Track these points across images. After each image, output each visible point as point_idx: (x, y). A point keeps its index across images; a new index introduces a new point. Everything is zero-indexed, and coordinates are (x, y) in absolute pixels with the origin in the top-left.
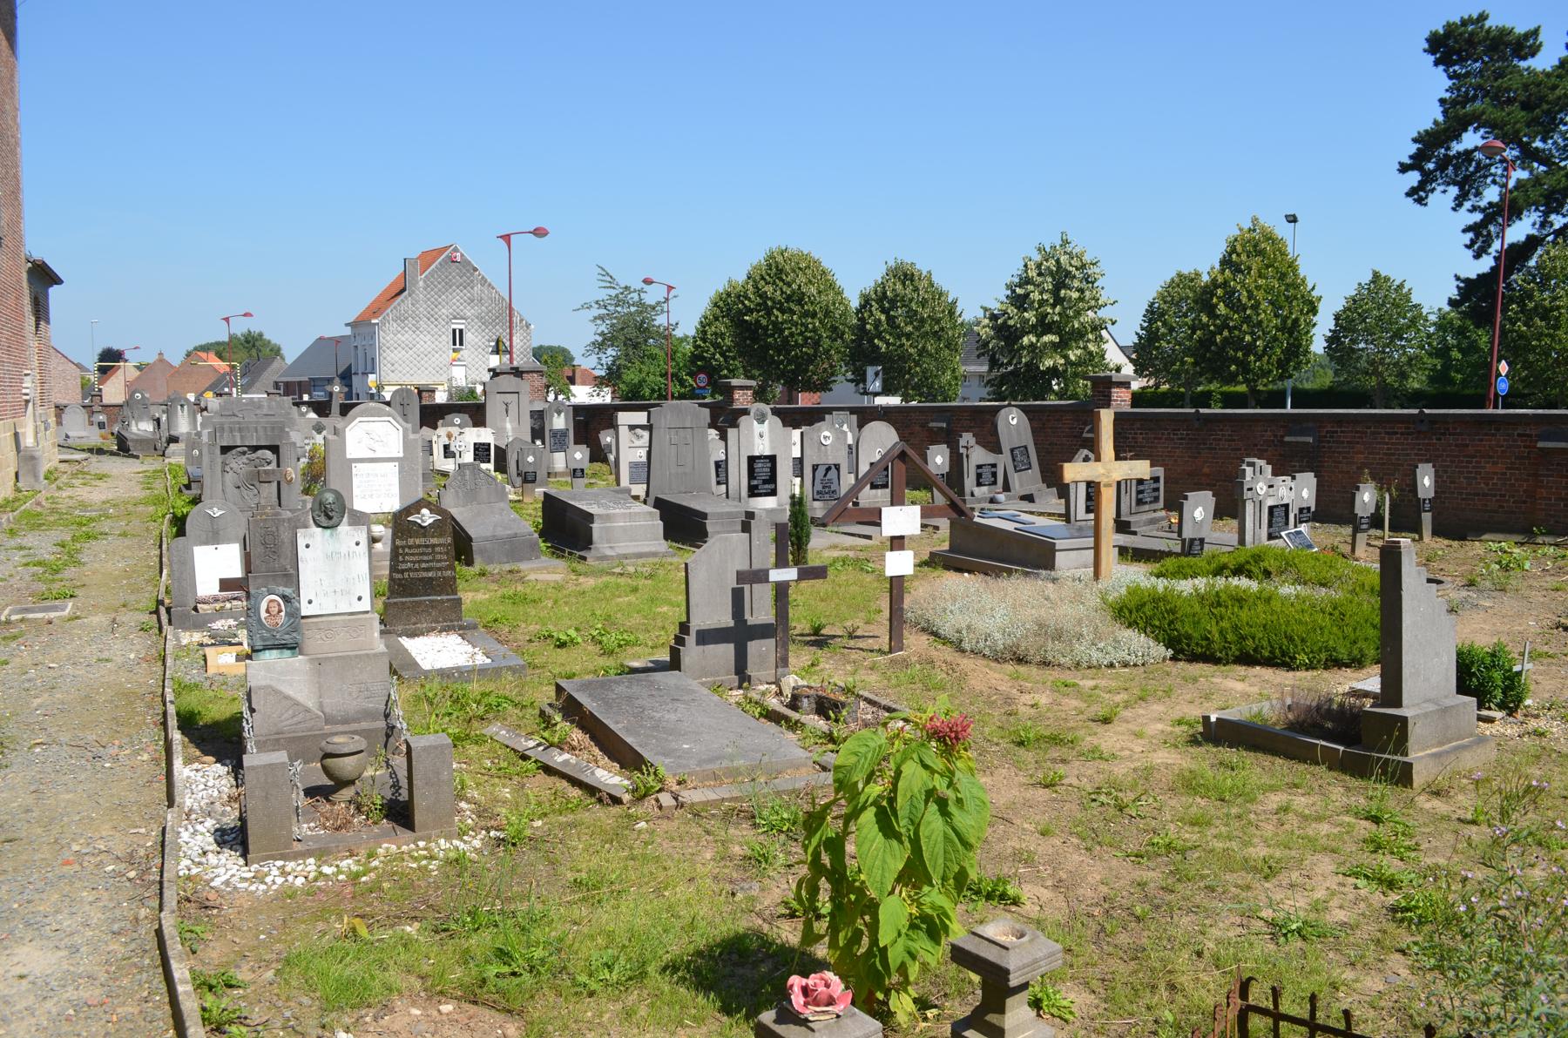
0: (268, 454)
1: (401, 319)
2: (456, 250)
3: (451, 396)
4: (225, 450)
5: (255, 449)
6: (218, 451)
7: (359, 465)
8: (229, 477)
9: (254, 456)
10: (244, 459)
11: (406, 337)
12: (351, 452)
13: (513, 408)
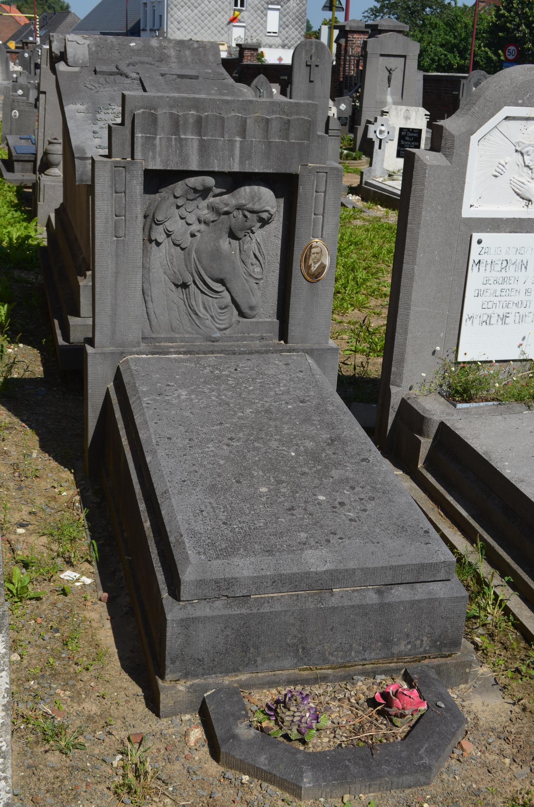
0: (266, 198)
3: (230, 53)
4: (157, 181)
5: (233, 181)
6: (137, 184)
7: (488, 238)
8: (162, 255)
9: (229, 200)
10: (202, 208)
12: (477, 202)
13: (397, 76)
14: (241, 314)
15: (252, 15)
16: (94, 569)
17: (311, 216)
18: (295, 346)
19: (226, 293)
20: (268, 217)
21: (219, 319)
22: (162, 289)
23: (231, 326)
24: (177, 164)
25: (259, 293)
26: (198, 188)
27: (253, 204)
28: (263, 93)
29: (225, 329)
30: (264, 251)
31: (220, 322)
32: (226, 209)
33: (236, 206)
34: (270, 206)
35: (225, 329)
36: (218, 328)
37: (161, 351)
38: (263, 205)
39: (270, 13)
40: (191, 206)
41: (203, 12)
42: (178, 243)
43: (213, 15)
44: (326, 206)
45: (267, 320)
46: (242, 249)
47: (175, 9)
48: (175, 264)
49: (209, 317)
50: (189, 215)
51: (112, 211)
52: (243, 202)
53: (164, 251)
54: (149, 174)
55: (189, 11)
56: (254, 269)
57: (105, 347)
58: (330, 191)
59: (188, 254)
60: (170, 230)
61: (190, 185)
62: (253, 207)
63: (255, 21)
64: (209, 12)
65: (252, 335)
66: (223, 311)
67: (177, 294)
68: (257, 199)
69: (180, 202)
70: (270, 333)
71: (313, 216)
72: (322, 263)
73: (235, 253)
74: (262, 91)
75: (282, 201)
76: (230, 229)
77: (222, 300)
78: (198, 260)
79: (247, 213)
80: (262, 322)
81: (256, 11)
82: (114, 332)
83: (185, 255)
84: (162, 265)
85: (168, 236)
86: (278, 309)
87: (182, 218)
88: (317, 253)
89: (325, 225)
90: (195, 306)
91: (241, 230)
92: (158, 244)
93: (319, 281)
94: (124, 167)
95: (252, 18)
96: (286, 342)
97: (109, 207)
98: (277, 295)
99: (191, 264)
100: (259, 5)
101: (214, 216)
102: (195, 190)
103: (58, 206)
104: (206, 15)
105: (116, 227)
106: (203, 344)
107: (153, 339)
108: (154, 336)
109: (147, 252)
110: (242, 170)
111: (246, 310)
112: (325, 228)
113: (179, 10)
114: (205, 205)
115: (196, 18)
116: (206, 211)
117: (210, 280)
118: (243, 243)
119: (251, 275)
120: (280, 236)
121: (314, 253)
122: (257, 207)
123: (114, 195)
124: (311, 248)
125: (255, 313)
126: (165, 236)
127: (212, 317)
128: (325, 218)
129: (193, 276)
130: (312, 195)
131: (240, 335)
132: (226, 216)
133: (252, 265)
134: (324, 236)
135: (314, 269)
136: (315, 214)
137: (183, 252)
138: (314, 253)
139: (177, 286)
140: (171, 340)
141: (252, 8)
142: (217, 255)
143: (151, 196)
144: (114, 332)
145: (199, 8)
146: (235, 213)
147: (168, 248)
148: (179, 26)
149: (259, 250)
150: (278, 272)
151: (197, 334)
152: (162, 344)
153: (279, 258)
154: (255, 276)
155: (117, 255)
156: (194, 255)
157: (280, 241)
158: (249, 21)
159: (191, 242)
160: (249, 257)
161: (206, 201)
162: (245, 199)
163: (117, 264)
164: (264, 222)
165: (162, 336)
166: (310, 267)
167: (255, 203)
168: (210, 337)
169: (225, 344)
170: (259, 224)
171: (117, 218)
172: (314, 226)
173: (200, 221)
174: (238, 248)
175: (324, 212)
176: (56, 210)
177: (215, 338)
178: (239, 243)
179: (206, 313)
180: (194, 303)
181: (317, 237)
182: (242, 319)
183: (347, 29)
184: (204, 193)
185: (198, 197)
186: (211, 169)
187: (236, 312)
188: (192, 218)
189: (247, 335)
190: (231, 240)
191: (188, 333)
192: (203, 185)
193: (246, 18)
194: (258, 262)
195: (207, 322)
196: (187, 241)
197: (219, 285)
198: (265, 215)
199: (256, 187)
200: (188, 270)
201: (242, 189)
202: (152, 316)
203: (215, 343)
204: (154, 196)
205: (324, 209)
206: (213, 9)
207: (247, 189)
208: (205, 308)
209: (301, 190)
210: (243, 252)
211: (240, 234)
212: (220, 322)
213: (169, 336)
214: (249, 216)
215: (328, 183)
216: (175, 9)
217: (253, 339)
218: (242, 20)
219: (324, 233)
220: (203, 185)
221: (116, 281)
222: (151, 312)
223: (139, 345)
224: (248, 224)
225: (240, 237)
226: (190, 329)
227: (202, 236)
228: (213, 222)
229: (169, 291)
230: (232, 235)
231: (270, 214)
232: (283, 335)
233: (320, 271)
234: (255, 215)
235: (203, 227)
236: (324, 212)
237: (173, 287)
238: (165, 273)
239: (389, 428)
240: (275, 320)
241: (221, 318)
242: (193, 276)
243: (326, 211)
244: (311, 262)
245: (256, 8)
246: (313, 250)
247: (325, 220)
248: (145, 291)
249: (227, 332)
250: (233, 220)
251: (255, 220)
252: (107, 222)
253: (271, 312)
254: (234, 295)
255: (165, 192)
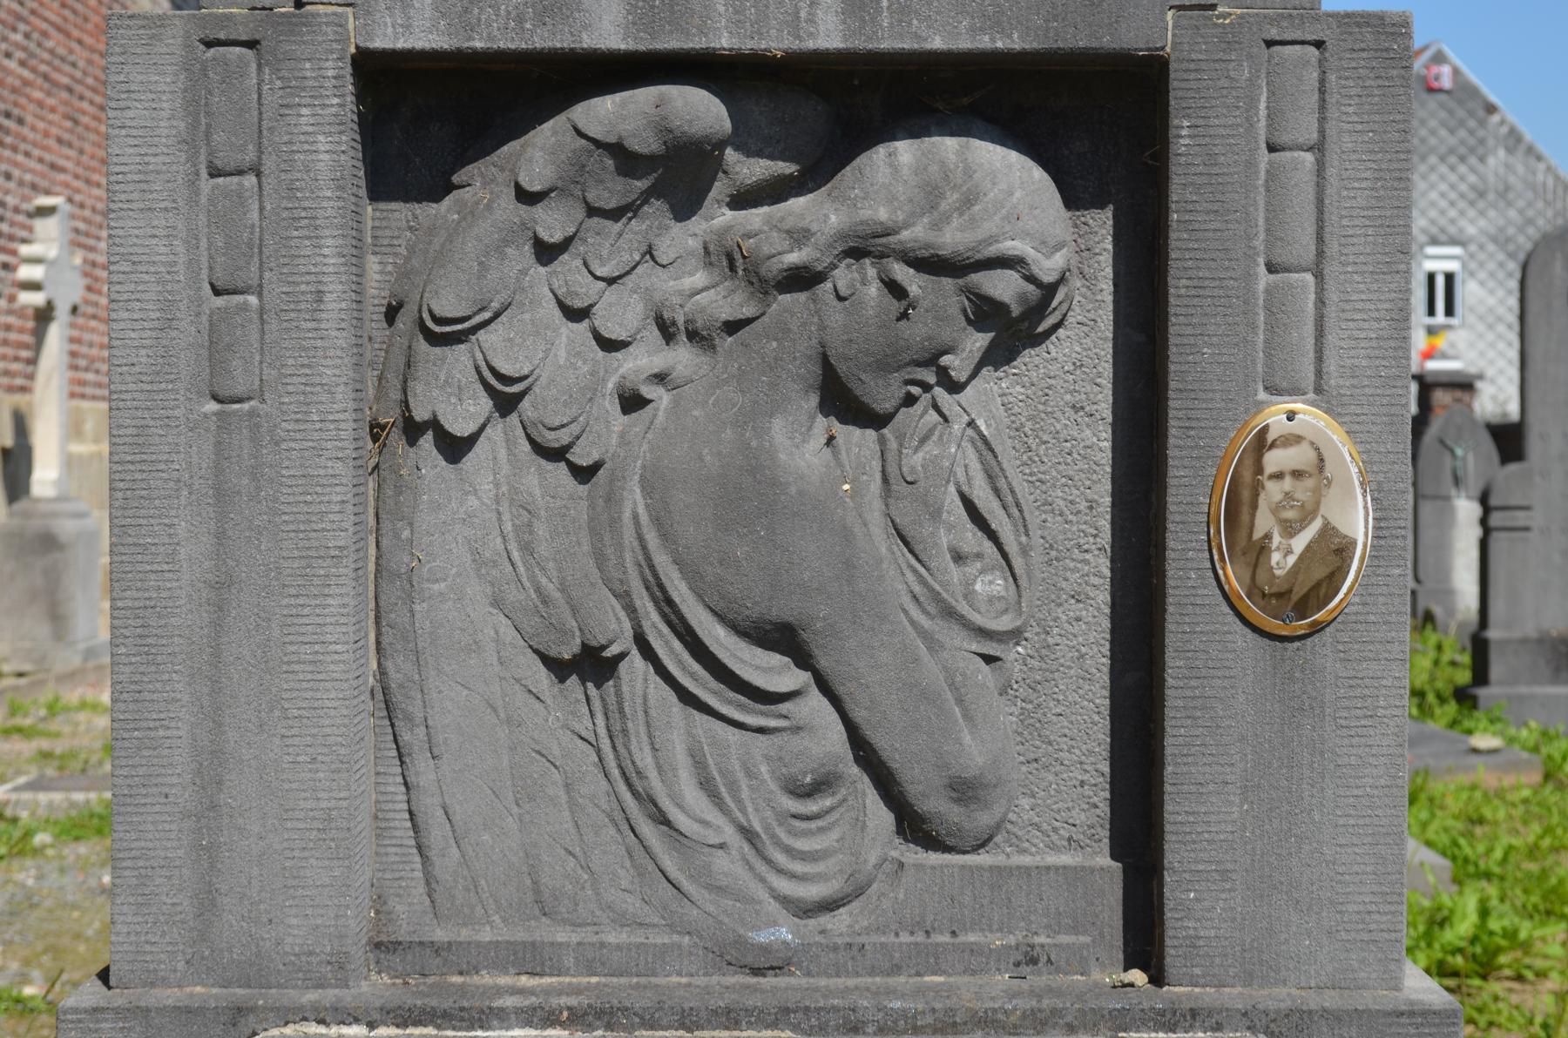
0: (1002, 195)
6: (322, 135)
8: (478, 506)
10: (679, 258)
14: (914, 827)
15: (1481, 336)
17: (1250, 277)
18: (1206, 995)
19: (816, 702)
20: (1022, 298)
21: (788, 851)
22: (482, 682)
23: (859, 892)
24: (520, 20)
25: (1006, 716)
26: (635, 145)
27: (936, 226)
28: (1464, 459)
29: (829, 906)
30: (1022, 489)
31: (798, 867)
32: (793, 258)
33: (842, 236)
34: (1026, 234)
35: (829, 906)
36: (785, 901)
37: (447, 1004)
38: (988, 227)
40: (611, 246)
42: (553, 439)
44: (1332, 218)
45: (1052, 859)
46: (892, 470)
48: (543, 550)
49: (730, 834)
50: (611, 294)
51: (192, 264)
52: (883, 214)
53: (486, 486)
54: (385, 81)
56: (969, 584)
57: (165, 983)
58: (1343, 142)
59: (608, 499)
60: (506, 368)
61: (594, 131)
62: (931, 237)
63: (1491, 354)
65: (972, 938)
66: (812, 807)
67: (564, 710)
68: (952, 198)
69: (552, 222)
70: (1075, 929)
71: (1263, 279)
72: (1328, 531)
73: (855, 493)
74: (1459, 452)
75: (1101, 222)
76: (825, 361)
77: (796, 742)
78: (657, 521)
79: (902, 273)
80: (1026, 871)
81: (1490, 327)
82: (207, 903)
83: (592, 506)
84: (479, 561)
85: (506, 404)
86: (1114, 803)
87: (575, 314)
88: (1297, 474)
89: (1330, 323)
90: (652, 774)
91: (885, 366)
92: (455, 448)
93: (1317, 629)
94: (251, 44)
95: (1481, 345)
96: (1157, 979)
97: (180, 249)
98: (1104, 723)
99: (620, 547)
101: (739, 297)
102: (624, 158)
105: (217, 348)
106: (701, 981)
107: (437, 949)
108: (440, 935)
109: (399, 491)
110: (860, 44)
111: (934, 804)
112: (1331, 339)
114: (692, 243)
116: (699, 278)
117: (721, 631)
118: (901, 438)
119: (950, 613)
120: (1105, 409)
121: (1278, 476)
122: (953, 239)
123: (206, 185)
124: (1261, 443)
125: (984, 819)
126: (486, 404)
127: (748, 834)
128: (1330, 285)
129: (631, 610)
130: (1251, 164)
131: (905, 938)
132: (802, 297)
133: (959, 558)
134: (1333, 382)
135: (1284, 558)
136: (1271, 268)
137: (583, 490)
138: (1278, 476)
139: (559, 668)
140: (532, 959)
141: (1481, 318)
142: (751, 493)
143: (417, 208)
144: (207, 903)
146: (844, 276)
147: (506, 469)
149: (991, 477)
150: (1103, 597)
151: (672, 927)
152: (486, 979)
153: (1105, 524)
154: (978, 619)
155: (222, 495)
156: (634, 499)
157: (1107, 434)
159: (622, 435)
160: (936, 514)
161: (697, 224)
162: (891, 199)
163: (220, 535)
164: (1013, 331)
165: (486, 935)
166: (1262, 549)
167: (946, 218)
168: (741, 943)
169: (823, 982)
170: (979, 341)
171: (220, 301)
172: (1271, 328)
173: (667, 330)
174: (876, 465)
175: (1320, 254)
177: (765, 949)
178: (882, 441)
179: (713, 815)
180: (645, 759)
181: (1295, 392)
182: (915, 855)
184: (680, 175)
185: (646, 197)
186: (697, 43)
187: (881, 817)
188: (621, 312)
189: (945, 938)
190: (838, 428)
191: (622, 920)
192: (663, 129)
193: (1462, 346)
194: (988, 547)
195: (721, 862)
196: (605, 433)
197: (776, 659)
198: (1004, 287)
199: (948, 146)
200: (607, 582)
201: (880, 152)
202: (437, 832)
203: (768, 981)
204: (432, 208)
205: (1320, 239)
207: (905, 151)
208: (707, 785)
209: (1183, 136)
210: (898, 487)
211: (881, 393)
212: (798, 867)
213: (521, 935)
214: (914, 290)
215: (1332, 99)
217: (976, 960)
218: (1451, 352)
219: (1331, 365)
220: (663, 129)
221: (218, 626)
222: (429, 805)
223: (340, 969)
224: (917, 331)
225: (885, 406)
226: (632, 904)
227: (676, 402)
228: (732, 327)
229: (521, 697)
230: (842, 401)
231: (1031, 279)
232: (1144, 942)
233: (1319, 573)
234: (947, 283)
235: (682, 358)
236: (1320, 254)
237: (542, 677)
238: (497, 603)
240: (1104, 860)
241: (802, 844)
242: (631, 610)
243: (1332, 247)
244: (1264, 522)
245: (1491, 319)
246: (1274, 460)
247: (1333, 296)
248: (397, 697)
249: (838, 923)
250: (836, 316)
251: (955, 311)
252: (168, 323)
253: (1080, 817)
254: (859, 715)
255: (484, 186)
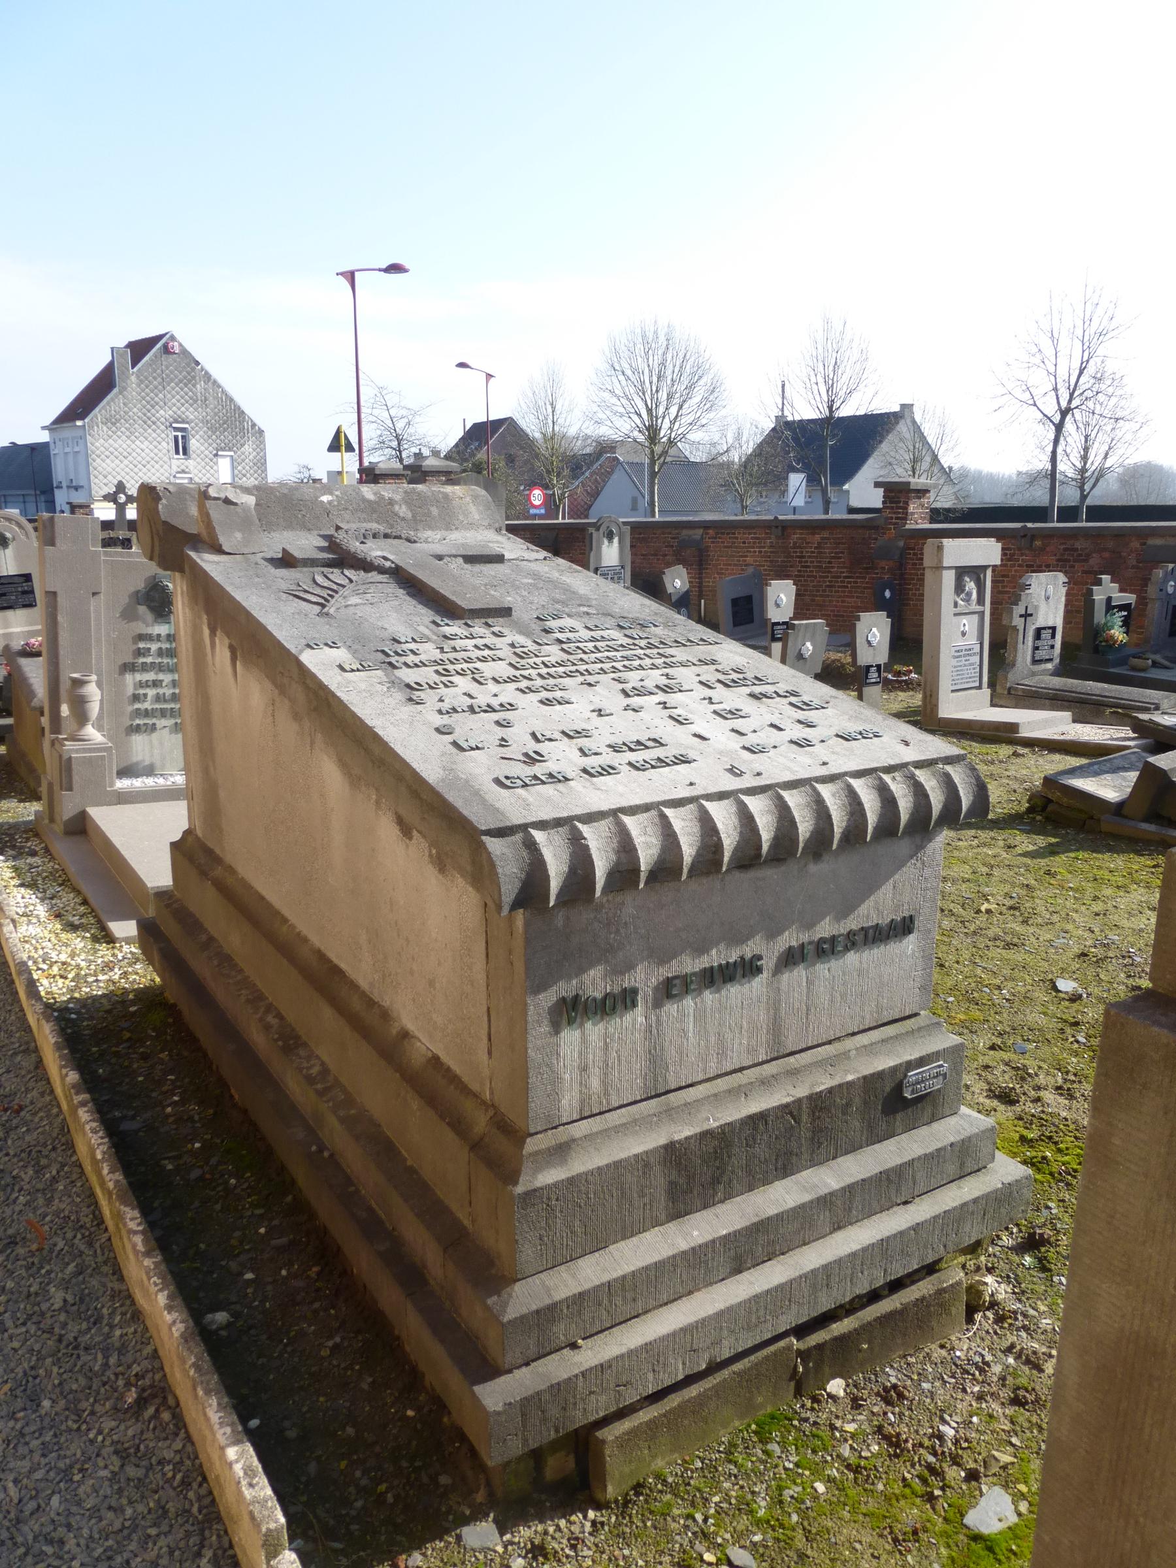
1: (112, 421)
2: (173, 338)
11: (120, 443)
16: (158, 1252)
39: (220, 460)
41: (135, 462)
43: (148, 466)
47: (98, 460)
55: (117, 462)
64: (144, 462)
100: (207, 452)
103: (177, 836)
104: (140, 466)
113: (103, 461)
115: (127, 470)
145: (130, 458)
148: (105, 481)
158: (196, 471)
176: (172, 844)
183: (377, 472)
193: (191, 468)
206: (148, 459)
216: (98, 460)
239: (1112, 670)
